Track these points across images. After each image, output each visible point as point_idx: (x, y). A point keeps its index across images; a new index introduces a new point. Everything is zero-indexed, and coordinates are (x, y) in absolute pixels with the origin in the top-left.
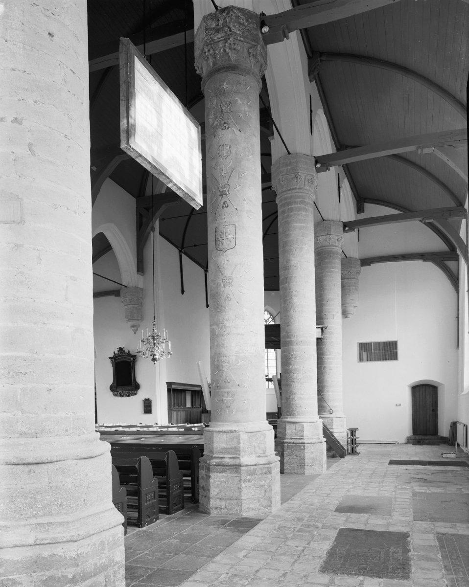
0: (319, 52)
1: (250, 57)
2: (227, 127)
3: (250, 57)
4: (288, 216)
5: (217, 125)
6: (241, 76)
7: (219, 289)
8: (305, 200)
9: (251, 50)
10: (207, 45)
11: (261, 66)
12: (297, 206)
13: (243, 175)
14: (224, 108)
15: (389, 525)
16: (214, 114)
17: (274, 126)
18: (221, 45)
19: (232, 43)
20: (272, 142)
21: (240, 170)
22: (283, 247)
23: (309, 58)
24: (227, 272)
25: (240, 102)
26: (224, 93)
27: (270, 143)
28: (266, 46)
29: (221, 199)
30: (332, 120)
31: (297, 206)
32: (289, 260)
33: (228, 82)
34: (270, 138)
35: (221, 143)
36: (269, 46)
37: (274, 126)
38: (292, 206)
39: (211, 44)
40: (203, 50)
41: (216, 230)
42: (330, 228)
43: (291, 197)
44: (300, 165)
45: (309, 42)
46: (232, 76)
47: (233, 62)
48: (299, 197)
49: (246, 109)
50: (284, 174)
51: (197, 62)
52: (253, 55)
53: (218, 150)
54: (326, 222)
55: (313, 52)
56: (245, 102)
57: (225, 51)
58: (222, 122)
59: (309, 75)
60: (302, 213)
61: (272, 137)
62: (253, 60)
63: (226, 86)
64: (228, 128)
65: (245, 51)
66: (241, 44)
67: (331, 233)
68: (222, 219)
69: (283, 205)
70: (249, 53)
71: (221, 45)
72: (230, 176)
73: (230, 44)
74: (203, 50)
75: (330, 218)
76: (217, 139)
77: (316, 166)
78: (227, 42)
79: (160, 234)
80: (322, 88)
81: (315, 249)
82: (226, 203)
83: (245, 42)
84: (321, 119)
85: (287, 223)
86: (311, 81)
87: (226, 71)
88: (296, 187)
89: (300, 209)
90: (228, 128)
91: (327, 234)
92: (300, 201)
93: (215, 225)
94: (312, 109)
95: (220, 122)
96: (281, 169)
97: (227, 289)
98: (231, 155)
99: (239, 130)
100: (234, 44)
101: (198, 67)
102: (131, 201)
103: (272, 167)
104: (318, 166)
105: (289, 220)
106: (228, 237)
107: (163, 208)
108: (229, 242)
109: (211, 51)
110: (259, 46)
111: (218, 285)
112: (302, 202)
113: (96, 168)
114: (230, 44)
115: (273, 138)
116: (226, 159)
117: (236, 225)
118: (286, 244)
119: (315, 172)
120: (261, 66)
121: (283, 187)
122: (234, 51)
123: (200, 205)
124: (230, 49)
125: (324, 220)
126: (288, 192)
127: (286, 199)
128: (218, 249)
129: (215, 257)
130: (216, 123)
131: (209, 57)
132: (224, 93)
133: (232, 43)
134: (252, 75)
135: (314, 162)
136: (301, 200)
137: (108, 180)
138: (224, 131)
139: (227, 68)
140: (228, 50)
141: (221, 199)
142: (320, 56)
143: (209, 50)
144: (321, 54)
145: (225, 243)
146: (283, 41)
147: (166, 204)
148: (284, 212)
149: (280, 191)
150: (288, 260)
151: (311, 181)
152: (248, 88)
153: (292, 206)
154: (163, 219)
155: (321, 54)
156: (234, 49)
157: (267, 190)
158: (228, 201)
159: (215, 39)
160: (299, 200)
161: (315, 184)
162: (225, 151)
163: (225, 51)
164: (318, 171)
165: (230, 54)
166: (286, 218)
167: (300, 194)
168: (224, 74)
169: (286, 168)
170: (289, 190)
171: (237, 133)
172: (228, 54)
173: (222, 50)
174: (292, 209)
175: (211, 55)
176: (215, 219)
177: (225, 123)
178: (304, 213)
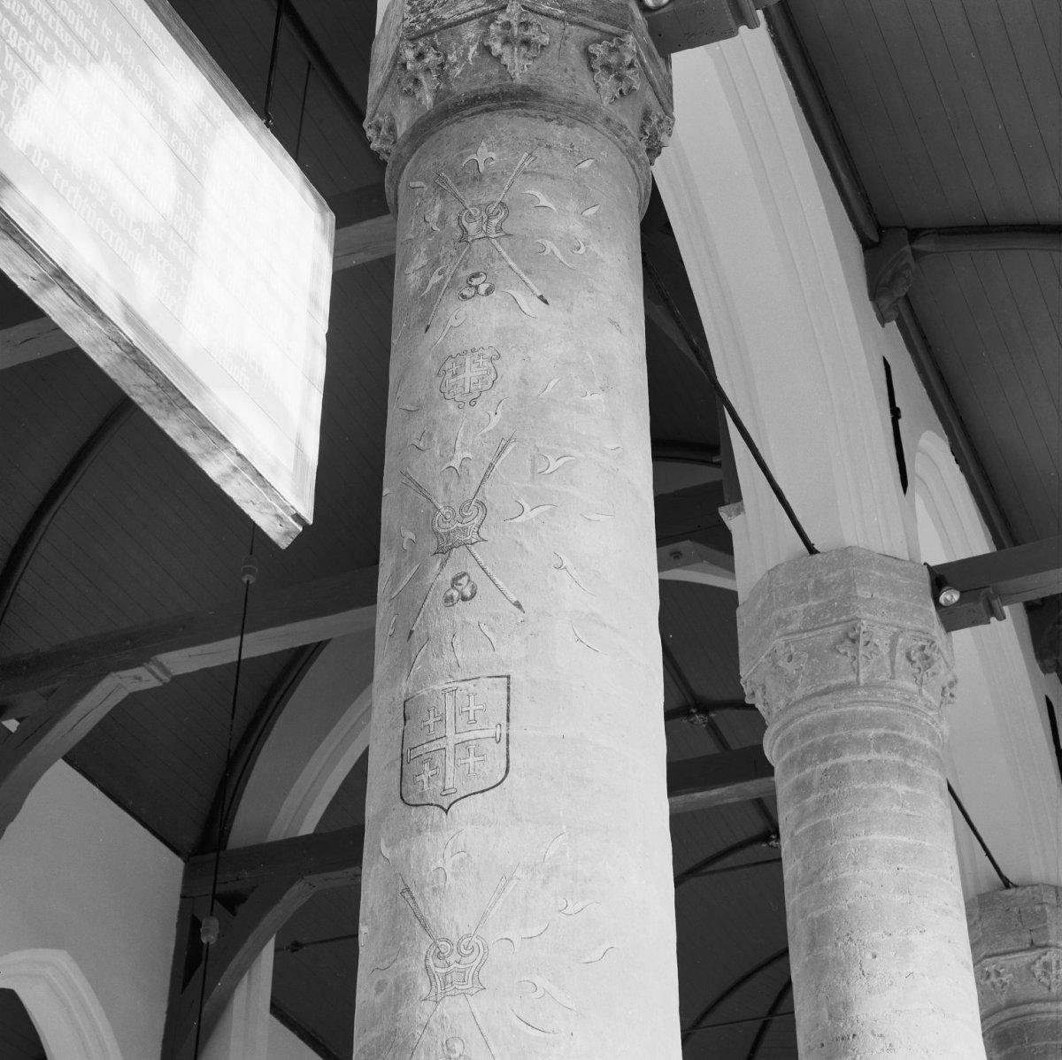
0: (905, 227)
1: (593, 70)
2: (483, 289)
3: (593, 70)
4: (824, 804)
5: (438, 286)
6: (552, 126)
7: (403, 1011)
8: (902, 734)
9: (599, 50)
10: (412, 40)
11: (646, 116)
12: (864, 757)
13: (554, 465)
14: (472, 228)
16: (429, 253)
18: (470, 32)
20: (734, 523)
21: (541, 444)
22: (813, 944)
23: (867, 246)
24: (454, 915)
25: (544, 201)
27: (727, 535)
28: (668, 62)
29: (442, 566)
30: (986, 477)
31: (864, 757)
32: (846, 1005)
33: (492, 146)
34: (723, 513)
35: (452, 348)
38: (841, 760)
39: (431, 33)
42: (1041, 918)
43: (835, 722)
44: (863, 592)
45: (858, 184)
46: (508, 125)
47: (519, 80)
48: (871, 721)
49: (577, 228)
50: (791, 627)
52: (607, 67)
53: (441, 372)
54: (1020, 893)
55: (880, 229)
56: (572, 205)
57: (486, 50)
58: (464, 274)
59: (874, 295)
60: (894, 787)
61: (733, 506)
62: (608, 83)
63: (485, 155)
64: (488, 292)
65: (574, 51)
66: (556, 26)
67: (1051, 941)
68: (440, 655)
69: (799, 761)
70: (589, 56)
71: (470, 32)
72: (491, 466)
73: (507, 25)
74: (398, 54)
75: (1038, 872)
76: (436, 336)
78: (492, 20)
79: (277, 1009)
80: (935, 363)
83: (572, 23)
84: (932, 450)
85: (821, 833)
86: (883, 320)
87: (487, 110)
88: (852, 678)
89: (879, 772)
90: (488, 292)
91: (1033, 946)
92: (878, 738)
93: (404, 686)
96: (782, 612)
97: (452, 1007)
98: (499, 386)
100: (525, 25)
101: (379, 129)
102: (155, 869)
103: (740, 611)
104: (950, 596)
105: (833, 818)
106: (466, 736)
107: (296, 895)
108: (471, 760)
109: (431, 57)
110: (631, 38)
111: (400, 992)
112: (883, 742)
113: (17, 723)
114: (507, 25)
115: (740, 511)
116: (473, 402)
118: (820, 930)
119: (937, 630)
120: (646, 116)
121: (792, 684)
122: (524, 49)
123: (298, 517)
124: (507, 41)
125: (1007, 884)
126: (819, 701)
127: (808, 731)
129: (392, 844)
130: (435, 279)
131: (421, 77)
132: (478, 178)
134: (600, 127)
135: (927, 585)
136: (882, 731)
137: (61, 767)
138: (468, 306)
139: (492, 97)
140: (497, 47)
141: (442, 566)
142: (911, 241)
143: (420, 56)
144: (915, 234)
145: (450, 763)
147: (309, 878)
148: (803, 788)
150: (839, 1008)
151: (924, 660)
152: (586, 165)
153: (841, 760)
154: (296, 946)
155: (915, 234)
157: (756, 847)
158: (476, 575)
160: (872, 733)
161: (944, 676)
162: (471, 373)
163: (488, 49)
164: (951, 620)
165: (505, 60)
166: (817, 812)
167: (876, 708)
168: (482, 120)
169: (801, 607)
170: (827, 692)
171: (530, 305)
172: (499, 58)
173: (473, 49)
174: (841, 773)
175: (428, 70)
176: (405, 662)
178: (902, 789)
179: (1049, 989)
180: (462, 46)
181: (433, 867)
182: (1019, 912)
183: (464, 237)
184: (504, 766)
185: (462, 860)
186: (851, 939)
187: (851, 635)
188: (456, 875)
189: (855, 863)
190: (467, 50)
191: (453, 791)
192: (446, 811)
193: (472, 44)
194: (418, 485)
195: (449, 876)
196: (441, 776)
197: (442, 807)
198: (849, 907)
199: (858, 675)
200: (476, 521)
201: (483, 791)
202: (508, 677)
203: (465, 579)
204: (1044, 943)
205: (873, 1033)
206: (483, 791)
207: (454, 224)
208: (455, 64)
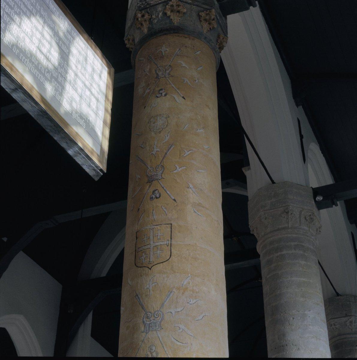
1: (201, 21)
2: (163, 94)
3: (201, 21)
5: (149, 93)
8: (303, 244)
9: (203, 14)
10: (141, 10)
11: (219, 36)
14: (160, 73)
15: (6, 88)
17: (245, 137)
19: (175, 4)
20: (247, 173)
26: (162, 57)
32: (284, 335)
33: (167, 46)
36: (230, 17)
37: (245, 137)
39: (147, 8)
40: (135, 15)
41: (138, 235)
46: (172, 39)
51: (128, 34)
52: (206, 20)
57: (165, 14)
58: (157, 89)
61: (247, 168)
63: (165, 49)
64: (165, 95)
70: (199, 16)
71: (160, 8)
72: (166, 153)
73: (172, 6)
74: (135, 15)
77: (315, 198)
81: (330, 340)
82: (157, 192)
84: (314, 150)
87: (165, 34)
88: (287, 225)
90: (165, 95)
91: (346, 315)
94: (302, 134)
95: (154, 89)
99: (183, 97)
100: (178, 6)
106: (157, 244)
109: (147, 16)
110: (213, 10)
115: (249, 169)
116: (160, 132)
117: (174, 224)
120: (219, 36)
122: (178, 14)
124: (172, 11)
125: (338, 295)
128: (138, 265)
130: (148, 91)
131: (143, 23)
132: (162, 57)
133: (175, 4)
136: (296, 243)
140: (169, 13)
141: (149, 187)
143: (143, 16)
145: (152, 253)
146: (249, 9)
149: (263, 234)
150: (282, 336)
151: (311, 219)
152: (198, 53)
156: (178, 12)
158: (161, 190)
159: (151, 3)
160: (293, 244)
162: (160, 122)
165: (171, 17)
167: (294, 236)
171: (179, 100)
172: (169, 17)
173: (161, 14)
175: (145, 21)
177: (161, 90)
178: (303, 262)
179: (352, 330)
180: (157, 13)
181: (146, 288)
182: (342, 304)
183: (157, 77)
184: (169, 254)
185: (155, 285)
186: (285, 313)
187: (286, 211)
188: (153, 291)
189: (287, 287)
190: (159, 14)
191: (152, 262)
192: (150, 269)
193: (160, 12)
194: (141, 160)
195: (151, 291)
196: (149, 257)
197: (149, 268)
198: (285, 302)
199: (288, 224)
200: (161, 172)
201: (163, 262)
202: (171, 224)
203: (157, 191)
204: (350, 314)
205: (293, 345)
206: (163, 262)
207: (154, 72)
208: (155, 19)
